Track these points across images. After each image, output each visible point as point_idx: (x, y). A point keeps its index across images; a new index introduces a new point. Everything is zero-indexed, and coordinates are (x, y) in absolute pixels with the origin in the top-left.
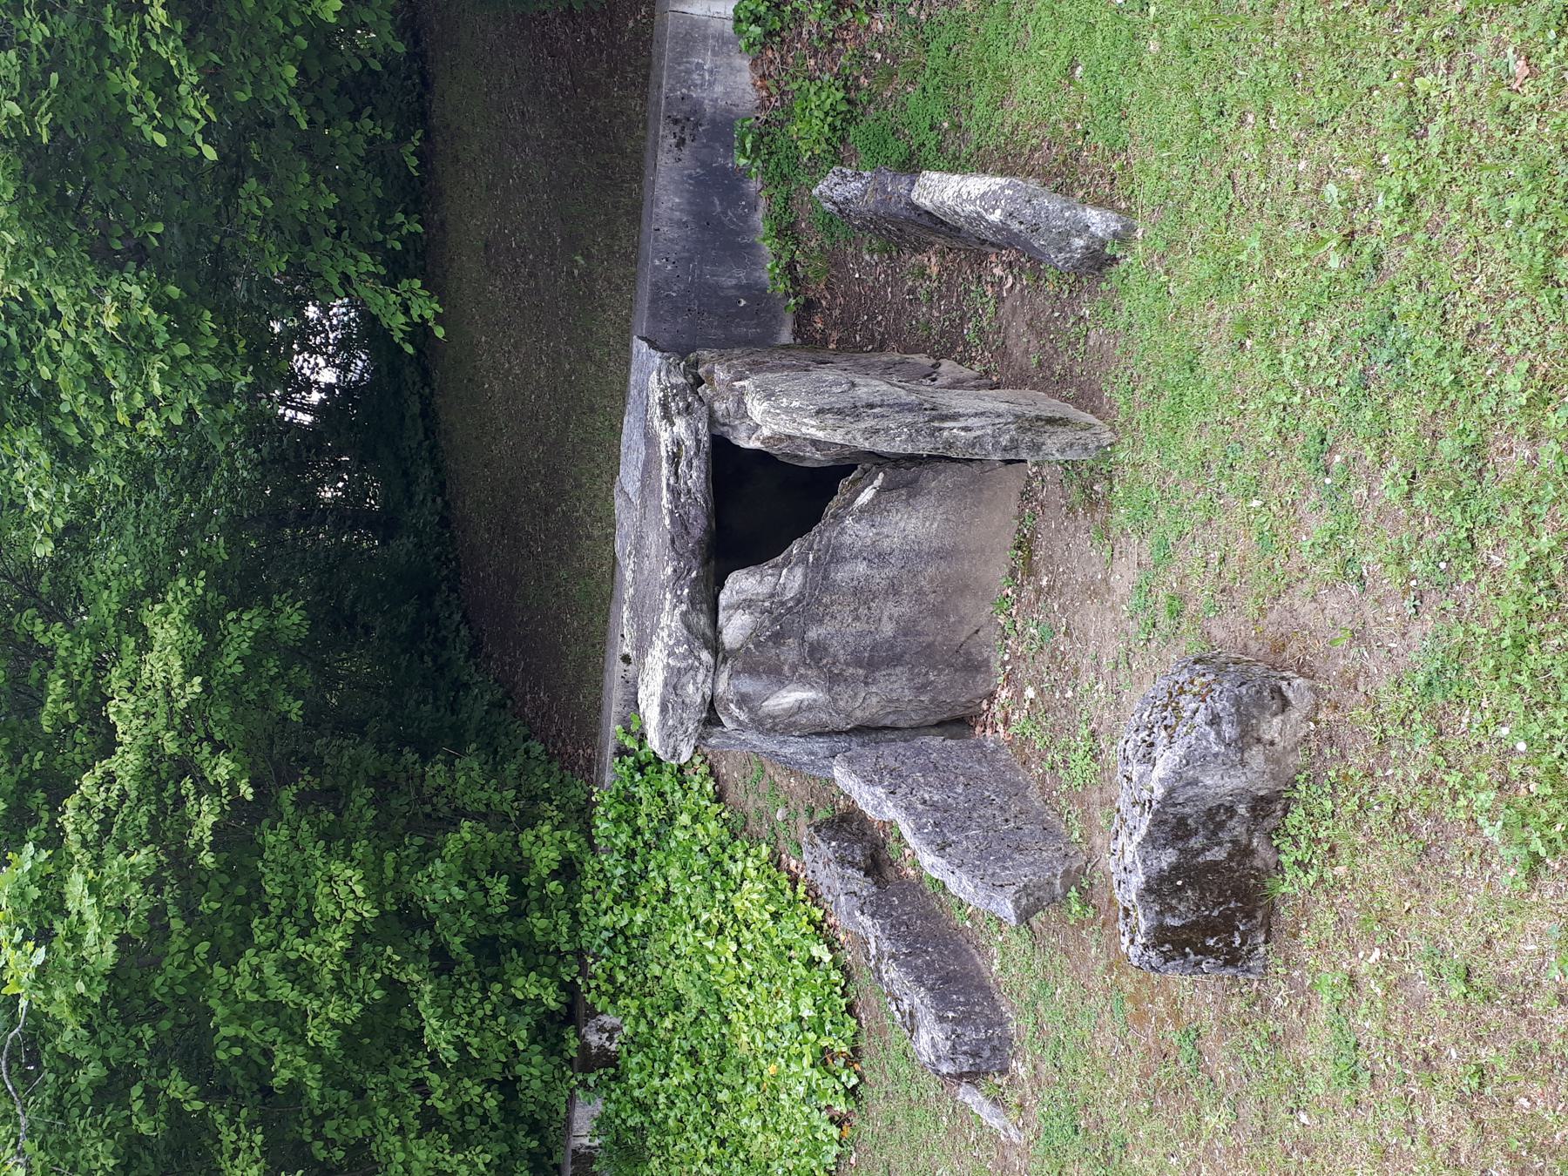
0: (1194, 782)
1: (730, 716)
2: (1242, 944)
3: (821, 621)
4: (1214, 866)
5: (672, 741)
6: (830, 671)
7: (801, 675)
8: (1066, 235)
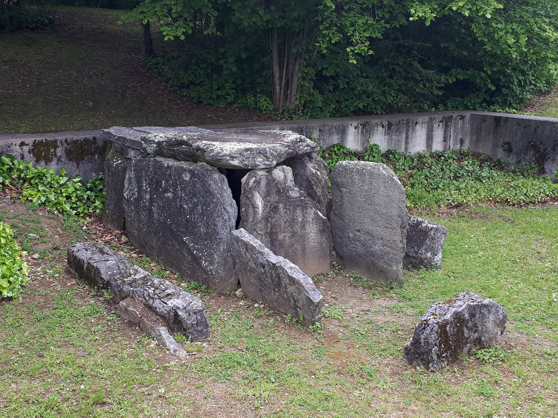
0: (489, 313)
1: (248, 179)
2: (444, 357)
3: (285, 208)
4: (463, 332)
5: (238, 156)
6: (269, 217)
7: (267, 205)
8: (432, 249)
